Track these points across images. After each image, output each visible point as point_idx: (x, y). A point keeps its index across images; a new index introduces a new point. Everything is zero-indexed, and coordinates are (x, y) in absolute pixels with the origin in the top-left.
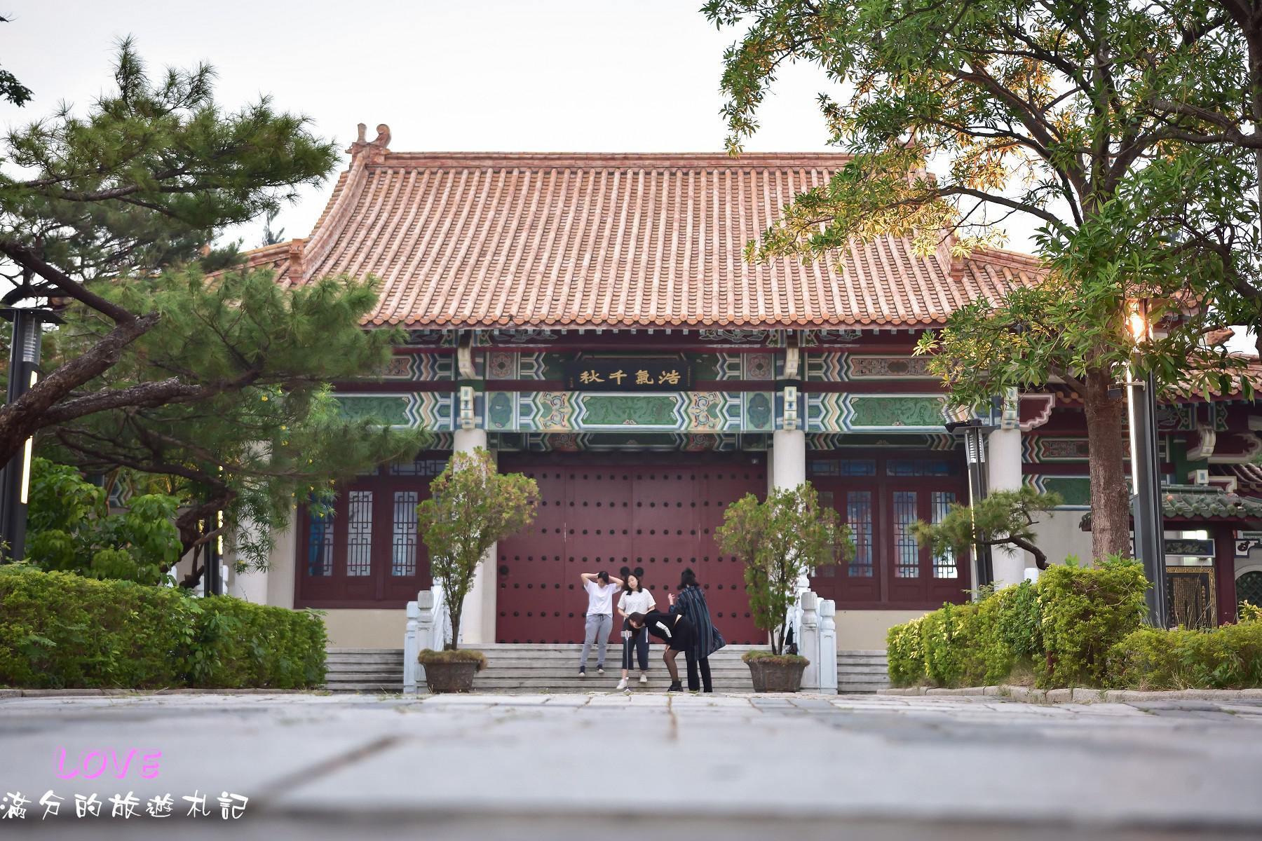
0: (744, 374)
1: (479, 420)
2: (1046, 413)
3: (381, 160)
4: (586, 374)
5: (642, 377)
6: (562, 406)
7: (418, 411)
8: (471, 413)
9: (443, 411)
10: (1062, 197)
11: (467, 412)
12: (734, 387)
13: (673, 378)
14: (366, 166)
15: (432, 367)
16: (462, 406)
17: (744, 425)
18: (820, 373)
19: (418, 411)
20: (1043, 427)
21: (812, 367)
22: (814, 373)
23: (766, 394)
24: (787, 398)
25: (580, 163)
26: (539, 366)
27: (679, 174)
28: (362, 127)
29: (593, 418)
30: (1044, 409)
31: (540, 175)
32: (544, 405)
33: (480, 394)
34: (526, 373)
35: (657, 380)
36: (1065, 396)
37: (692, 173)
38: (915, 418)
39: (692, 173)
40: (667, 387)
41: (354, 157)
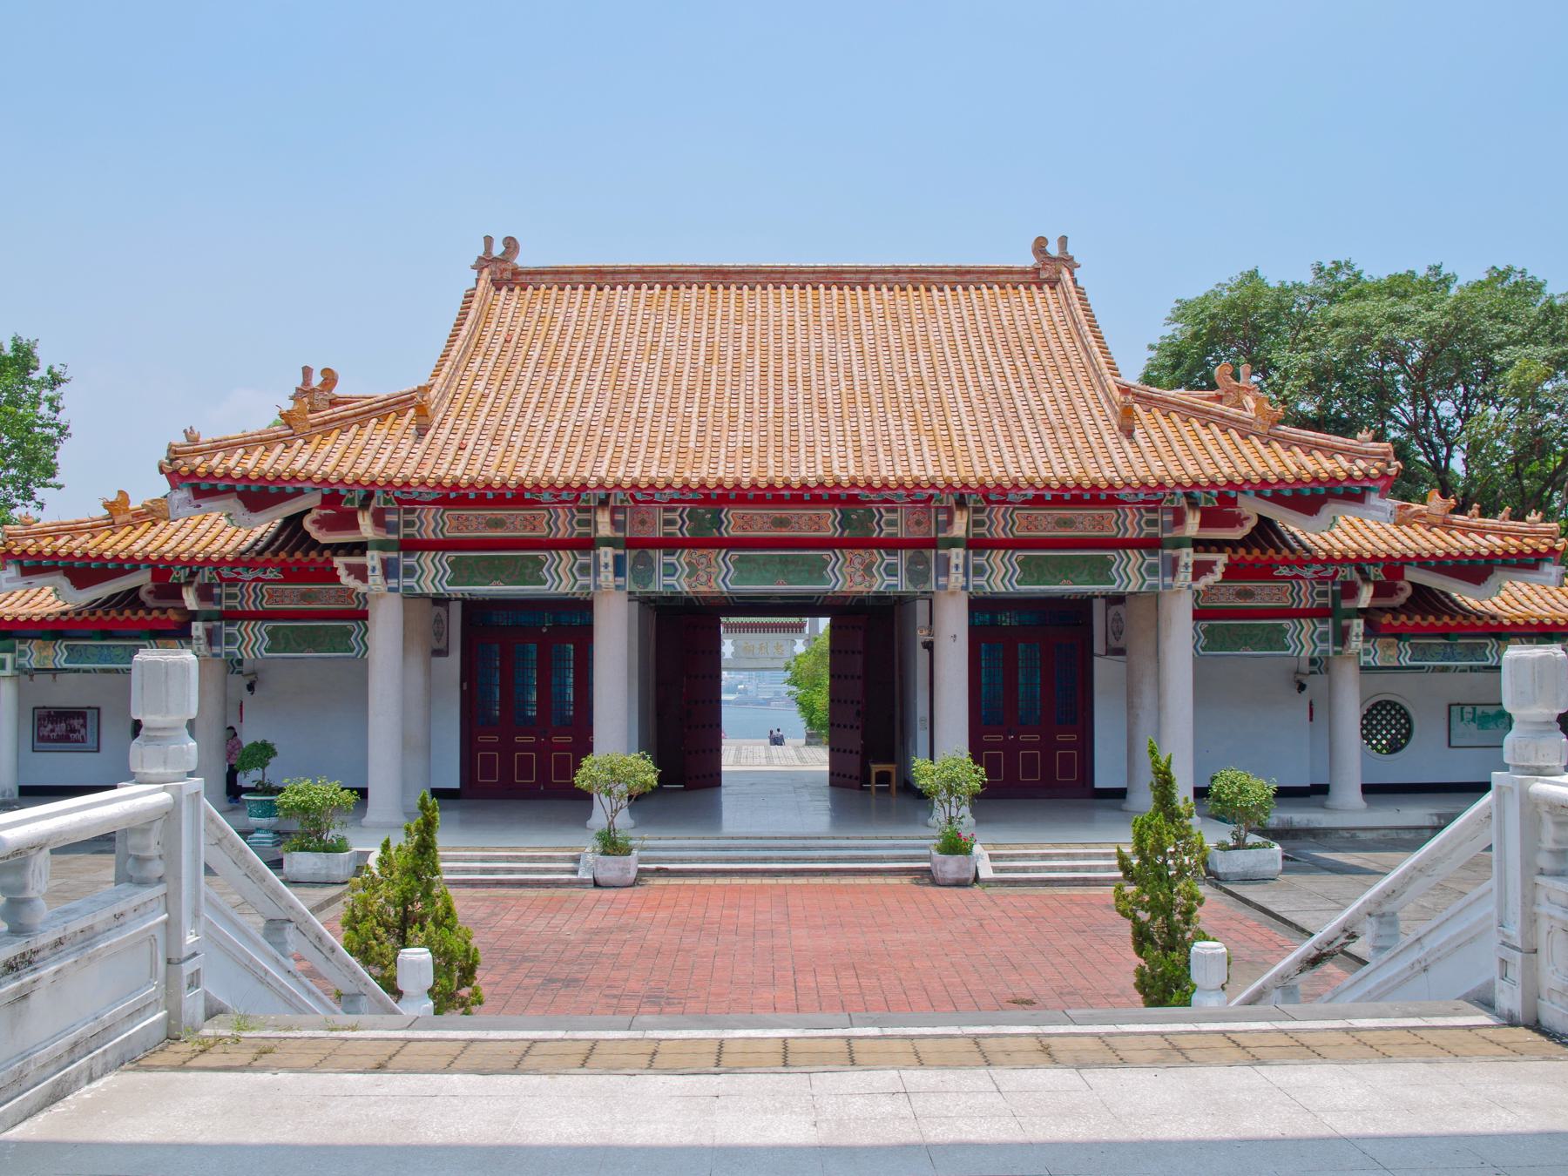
2: (1219, 570)
6: (709, 565)
9: (584, 569)
10: (1029, 261)
11: (607, 577)
12: (891, 545)
15: (570, 523)
17: (900, 584)
28: (488, 241)
41: (480, 272)
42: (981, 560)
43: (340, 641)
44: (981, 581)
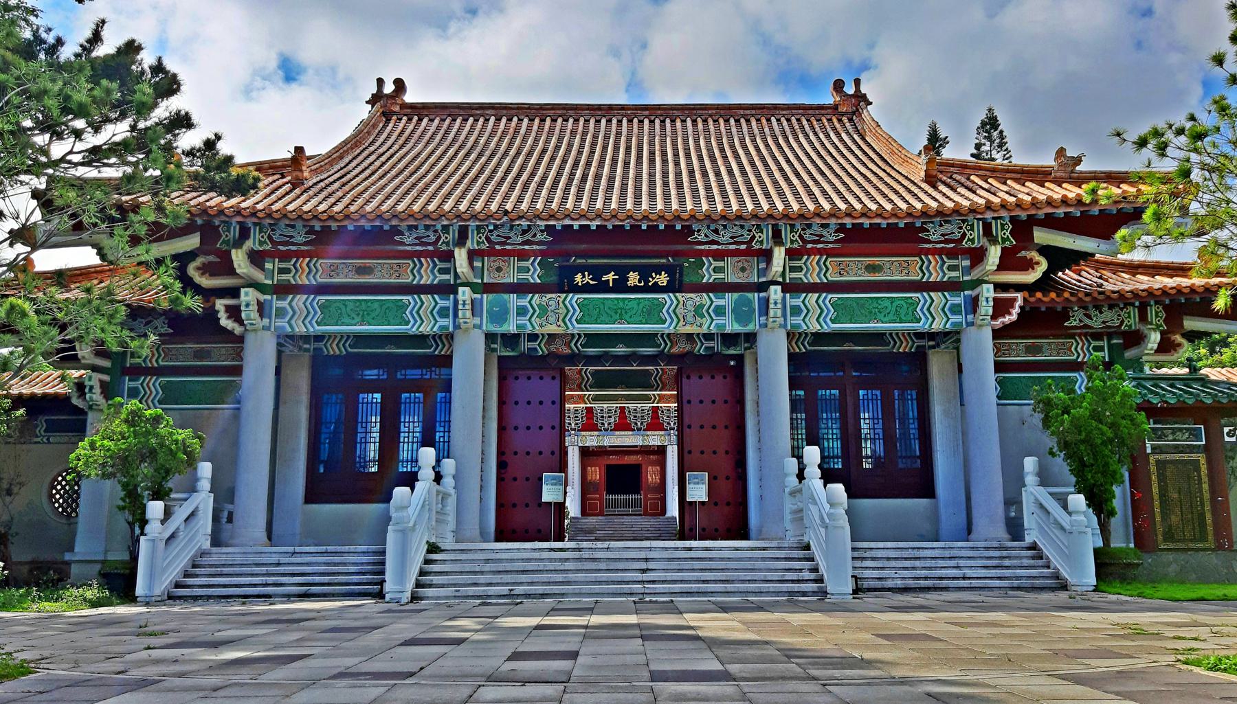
0: (731, 277)
1: (477, 320)
2: (1016, 311)
3: (397, 109)
4: (579, 276)
5: (633, 278)
7: (418, 312)
8: (469, 314)
13: (662, 279)
14: (383, 114)
15: (432, 271)
16: (460, 307)
18: (800, 275)
19: (928, 309)
20: (1012, 324)
21: (792, 269)
22: (794, 275)
23: (750, 295)
24: (773, 297)
25: (571, 112)
26: (535, 270)
27: (657, 121)
28: (380, 82)
29: (586, 319)
30: (1013, 307)
31: (537, 121)
32: (539, 306)
33: (479, 296)
34: (523, 276)
35: (647, 282)
36: (1058, 296)
37: (668, 121)
38: (891, 317)
39: (668, 121)
40: (656, 289)
42: (797, 301)
43: (217, 395)
44: (798, 320)
